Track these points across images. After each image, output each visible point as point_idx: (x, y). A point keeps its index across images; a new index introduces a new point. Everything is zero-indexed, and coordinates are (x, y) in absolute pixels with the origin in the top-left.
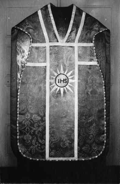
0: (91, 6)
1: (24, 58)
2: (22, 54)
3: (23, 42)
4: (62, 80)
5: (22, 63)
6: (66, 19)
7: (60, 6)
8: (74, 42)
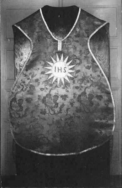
0: (95, 6)
1: (23, 61)
2: (21, 57)
3: (21, 44)
4: (59, 69)
5: (21, 66)
6: (59, 16)
7: (59, 6)
8: (89, 69)
